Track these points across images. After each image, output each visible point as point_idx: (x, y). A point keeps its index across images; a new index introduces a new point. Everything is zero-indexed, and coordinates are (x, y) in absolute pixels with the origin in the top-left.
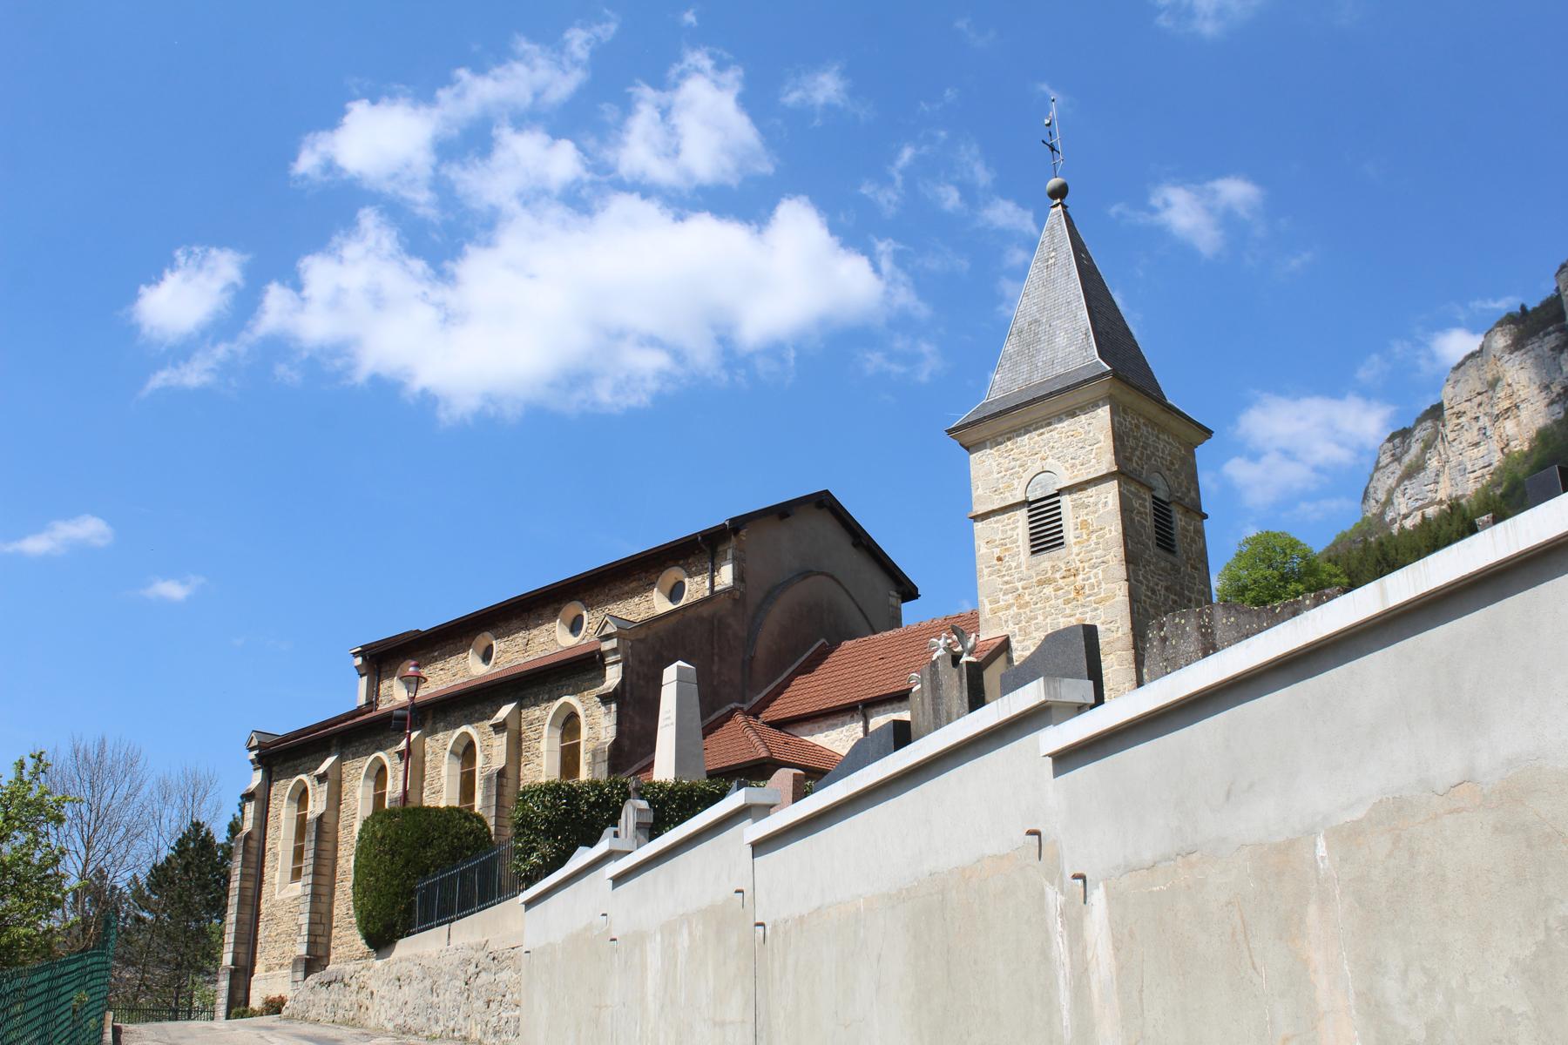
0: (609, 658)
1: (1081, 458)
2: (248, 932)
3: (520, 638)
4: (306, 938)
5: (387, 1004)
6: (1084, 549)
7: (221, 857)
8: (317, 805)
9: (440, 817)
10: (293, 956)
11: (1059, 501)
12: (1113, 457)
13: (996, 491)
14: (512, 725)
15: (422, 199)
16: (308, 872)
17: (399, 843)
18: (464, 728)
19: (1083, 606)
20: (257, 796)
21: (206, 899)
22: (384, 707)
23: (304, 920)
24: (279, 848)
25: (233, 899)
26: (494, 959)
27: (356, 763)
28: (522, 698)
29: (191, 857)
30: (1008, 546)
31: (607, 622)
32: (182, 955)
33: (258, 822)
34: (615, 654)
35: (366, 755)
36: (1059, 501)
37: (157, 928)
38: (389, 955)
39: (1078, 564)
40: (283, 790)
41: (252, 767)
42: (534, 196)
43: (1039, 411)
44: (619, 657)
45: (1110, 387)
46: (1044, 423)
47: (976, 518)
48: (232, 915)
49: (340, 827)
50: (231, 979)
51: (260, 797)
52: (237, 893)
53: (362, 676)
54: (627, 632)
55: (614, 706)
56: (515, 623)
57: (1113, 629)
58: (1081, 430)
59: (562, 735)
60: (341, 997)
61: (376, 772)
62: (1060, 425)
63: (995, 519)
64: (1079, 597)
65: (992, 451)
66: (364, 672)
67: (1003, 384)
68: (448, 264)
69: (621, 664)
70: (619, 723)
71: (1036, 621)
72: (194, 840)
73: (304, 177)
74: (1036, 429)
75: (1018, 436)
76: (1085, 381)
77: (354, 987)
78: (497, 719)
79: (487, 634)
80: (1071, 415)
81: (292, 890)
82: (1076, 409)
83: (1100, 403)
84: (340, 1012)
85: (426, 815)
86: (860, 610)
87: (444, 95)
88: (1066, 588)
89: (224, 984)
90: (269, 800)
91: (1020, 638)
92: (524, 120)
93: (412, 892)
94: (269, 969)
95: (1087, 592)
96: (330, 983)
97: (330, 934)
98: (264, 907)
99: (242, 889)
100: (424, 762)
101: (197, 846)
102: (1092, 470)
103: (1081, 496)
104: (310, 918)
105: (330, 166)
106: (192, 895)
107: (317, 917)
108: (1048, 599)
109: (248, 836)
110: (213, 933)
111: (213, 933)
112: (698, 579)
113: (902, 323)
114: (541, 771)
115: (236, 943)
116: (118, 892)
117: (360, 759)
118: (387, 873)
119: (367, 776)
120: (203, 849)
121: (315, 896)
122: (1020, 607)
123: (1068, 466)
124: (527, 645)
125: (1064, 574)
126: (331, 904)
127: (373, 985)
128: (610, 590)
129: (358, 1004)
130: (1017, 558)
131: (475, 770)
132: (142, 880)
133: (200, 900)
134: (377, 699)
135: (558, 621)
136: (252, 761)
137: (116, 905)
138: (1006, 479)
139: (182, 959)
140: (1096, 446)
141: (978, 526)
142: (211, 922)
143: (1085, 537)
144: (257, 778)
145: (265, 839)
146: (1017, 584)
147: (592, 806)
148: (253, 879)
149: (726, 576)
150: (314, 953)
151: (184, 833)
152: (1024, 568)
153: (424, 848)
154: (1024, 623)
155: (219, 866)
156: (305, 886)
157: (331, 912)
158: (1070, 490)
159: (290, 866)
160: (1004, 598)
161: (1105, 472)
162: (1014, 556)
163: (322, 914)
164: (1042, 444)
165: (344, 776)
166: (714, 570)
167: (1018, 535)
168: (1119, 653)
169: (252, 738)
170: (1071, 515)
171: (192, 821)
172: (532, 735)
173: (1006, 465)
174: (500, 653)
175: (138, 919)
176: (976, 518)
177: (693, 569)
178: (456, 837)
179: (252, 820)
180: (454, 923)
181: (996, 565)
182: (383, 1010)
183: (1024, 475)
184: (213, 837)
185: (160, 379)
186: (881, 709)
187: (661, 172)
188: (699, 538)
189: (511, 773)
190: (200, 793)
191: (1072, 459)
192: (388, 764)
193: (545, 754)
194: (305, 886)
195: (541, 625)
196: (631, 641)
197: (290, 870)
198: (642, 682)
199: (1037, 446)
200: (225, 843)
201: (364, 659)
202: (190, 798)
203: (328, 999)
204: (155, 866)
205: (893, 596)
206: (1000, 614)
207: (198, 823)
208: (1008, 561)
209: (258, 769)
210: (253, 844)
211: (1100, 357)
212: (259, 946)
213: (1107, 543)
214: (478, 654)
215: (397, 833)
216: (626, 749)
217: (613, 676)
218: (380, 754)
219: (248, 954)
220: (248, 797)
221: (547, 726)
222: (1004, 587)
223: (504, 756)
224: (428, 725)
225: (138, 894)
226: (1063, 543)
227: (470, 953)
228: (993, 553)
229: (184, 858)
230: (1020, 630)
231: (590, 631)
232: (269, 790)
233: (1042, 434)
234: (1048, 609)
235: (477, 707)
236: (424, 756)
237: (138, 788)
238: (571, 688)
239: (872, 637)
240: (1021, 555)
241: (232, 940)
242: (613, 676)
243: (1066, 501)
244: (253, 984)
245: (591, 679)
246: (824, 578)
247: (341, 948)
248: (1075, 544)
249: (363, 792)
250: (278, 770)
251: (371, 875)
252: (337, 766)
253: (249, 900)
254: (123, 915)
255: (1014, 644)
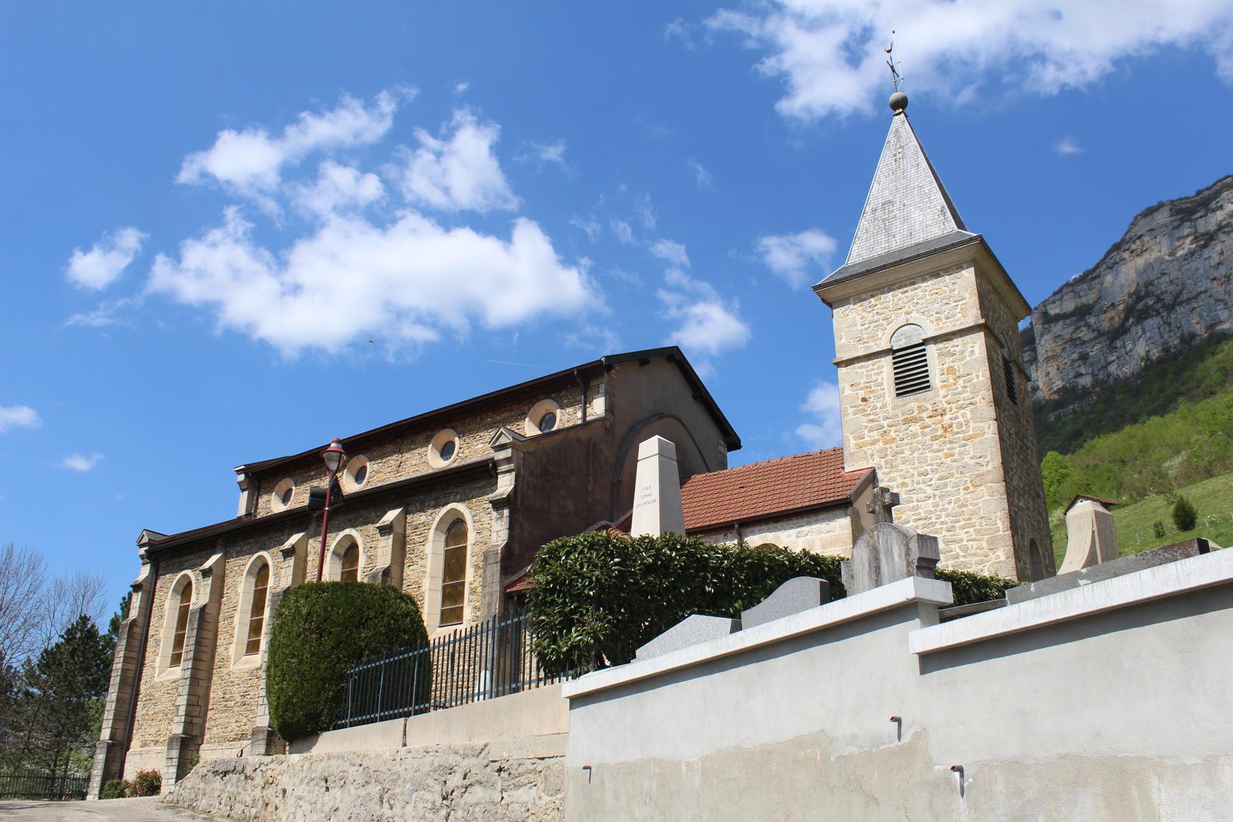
0: (502, 467)
1: (946, 313)
2: (127, 710)
3: (393, 460)
4: (183, 719)
5: (307, 807)
6: (950, 392)
7: (102, 645)
8: (200, 596)
9: (375, 594)
10: (169, 735)
11: (924, 350)
12: (979, 312)
13: (860, 340)
14: (398, 529)
15: (270, 206)
16: (189, 657)
17: (329, 621)
18: (347, 531)
19: (951, 442)
20: (144, 588)
21: (87, 679)
22: (261, 514)
23: (182, 701)
24: (161, 635)
25: (115, 680)
26: (500, 770)
27: (240, 561)
28: (408, 505)
29: (78, 645)
30: (873, 388)
31: (502, 433)
32: (63, 726)
33: (143, 611)
34: (509, 464)
35: (249, 554)
36: (924, 350)
37: (45, 698)
38: (309, 749)
39: (945, 405)
40: (168, 584)
41: (141, 561)
42: (348, 209)
43: (905, 271)
44: (512, 466)
45: (976, 251)
46: (908, 282)
47: (839, 364)
48: (112, 694)
49: (221, 618)
50: (108, 752)
51: (147, 590)
52: (119, 674)
53: (243, 490)
54: (521, 444)
55: (506, 512)
56: (389, 448)
57: (983, 463)
58: (946, 288)
59: (447, 540)
60: (240, 790)
61: (258, 570)
62: (925, 284)
63: (859, 365)
64: (947, 435)
65: (856, 307)
66: (245, 487)
67: (865, 248)
68: (283, 252)
69: (514, 473)
70: (511, 528)
71: (903, 455)
72: (81, 631)
73: (185, 186)
74: (899, 288)
75: (881, 294)
76: (953, 245)
77: (259, 780)
78: (384, 522)
79: (362, 457)
80: (935, 276)
81: (171, 673)
82: (939, 270)
83: (965, 266)
84: (238, 808)
85: (360, 591)
86: (700, 452)
87: (291, 131)
88: (933, 426)
89: (101, 757)
90: (154, 591)
91: (887, 470)
92: (343, 155)
93: (343, 677)
94: (144, 744)
95: (955, 430)
96: (225, 773)
97: (206, 715)
98: (143, 688)
99: (124, 670)
100: (306, 561)
101: (83, 636)
102: (958, 323)
103: (947, 345)
104: (188, 700)
105: (204, 175)
106: (76, 676)
107: (194, 699)
108: (915, 436)
109: (134, 623)
110: (91, 708)
111: (91, 708)
112: (570, 410)
113: (594, 318)
114: (424, 572)
115: (115, 720)
116: (13, 671)
117: (243, 557)
118: (313, 654)
119: (249, 573)
120: (87, 638)
121: (194, 680)
122: (886, 443)
123: (933, 319)
124: (399, 466)
125: (931, 414)
126: (208, 688)
127: (285, 781)
128: (482, 419)
129: (264, 801)
130: (882, 399)
131: (357, 570)
132: (35, 661)
133: (82, 680)
134: (256, 511)
135: (430, 446)
136: (142, 557)
137: (10, 681)
138: (870, 330)
139: (63, 728)
140: (961, 302)
141: (842, 371)
142: (90, 699)
143: (952, 381)
144: (145, 572)
145: (148, 626)
146: (882, 422)
147: (648, 569)
148: (135, 662)
149: (598, 407)
150: (190, 733)
151: (73, 625)
152: (889, 408)
153: (357, 628)
154: (890, 457)
155: (100, 653)
156: (185, 670)
157: (208, 695)
158: (935, 340)
159: (170, 652)
160: (868, 434)
161: (972, 324)
162: (879, 398)
163: (199, 696)
164: (906, 300)
165: (227, 572)
166: (587, 402)
167: (882, 379)
168: (990, 484)
169: (143, 535)
170: (937, 361)
171: (80, 615)
172: (417, 539)
173: (870, 319)
174: (374, 473)
175: (27, 694)
176: (839, 364)
177: (565, 401)
178: (393, 619)
179: (138, 609)
180: (412, 718)
181: (861, 405)
182: (299, 813)
183: (888, 327)
184: (97, 630)
185: (76, 319)
186: (756, 529)
187: (437, 199)
188: (576, 372)
189: (395, 572)
190: (89, 593)
191: (936, 313)
192: (270, 563)
193: (430, 556)
194: (185, 670)
195: (413, 449)
196: (524, 453)
197: (170, 656)
198: (531, 492)
199: (900, 302)
200: (107, 635)
201: (247, 476)
202: (81, 598)
203: (223, 790)
204: (46, 651)
205: (721, 445)
206: (866, 449)
207: (85, 617)
208: (873, 402)
209: (146, 563)
210: (137, 630)
211: (959, 228)
212: (136, 723)
213: (975, 387)
214: (352, 475)
215: (326, 610)
216: (516, 553)
217: (505, 484)
218: (264, 553)
219: (125, 729)
220: (137, 587)
221: (432, 531)
222: (869, 425)
223: (389, 557)
224: (312, 527)
225: (30, 674)
226: (929, 387)
227: (452, 760)
228: (857, 394)
229: (72, 645)
230: (886, 463)
231: (461, 455)
232: (156, 583)
233: (906, 292)
234: (915, 445)
235: (362, 512)
236: (307, 556)
237: (38, 588)
238: (458, 496)
239: (722, 472)
240: (887, 397)
241: (112, 717)
242: (505, 484)
243: (931, 350)
244: (129, 758)
245: (480, 488)
246: (672, 420)
247: (215, 729)
248: (942, 387)
249: (245, 587)
250: (164, 566)
251: (294, 656)
252: (222, 563)
253: (130, 681)
254: (15, 690)
255: (880, 475)
